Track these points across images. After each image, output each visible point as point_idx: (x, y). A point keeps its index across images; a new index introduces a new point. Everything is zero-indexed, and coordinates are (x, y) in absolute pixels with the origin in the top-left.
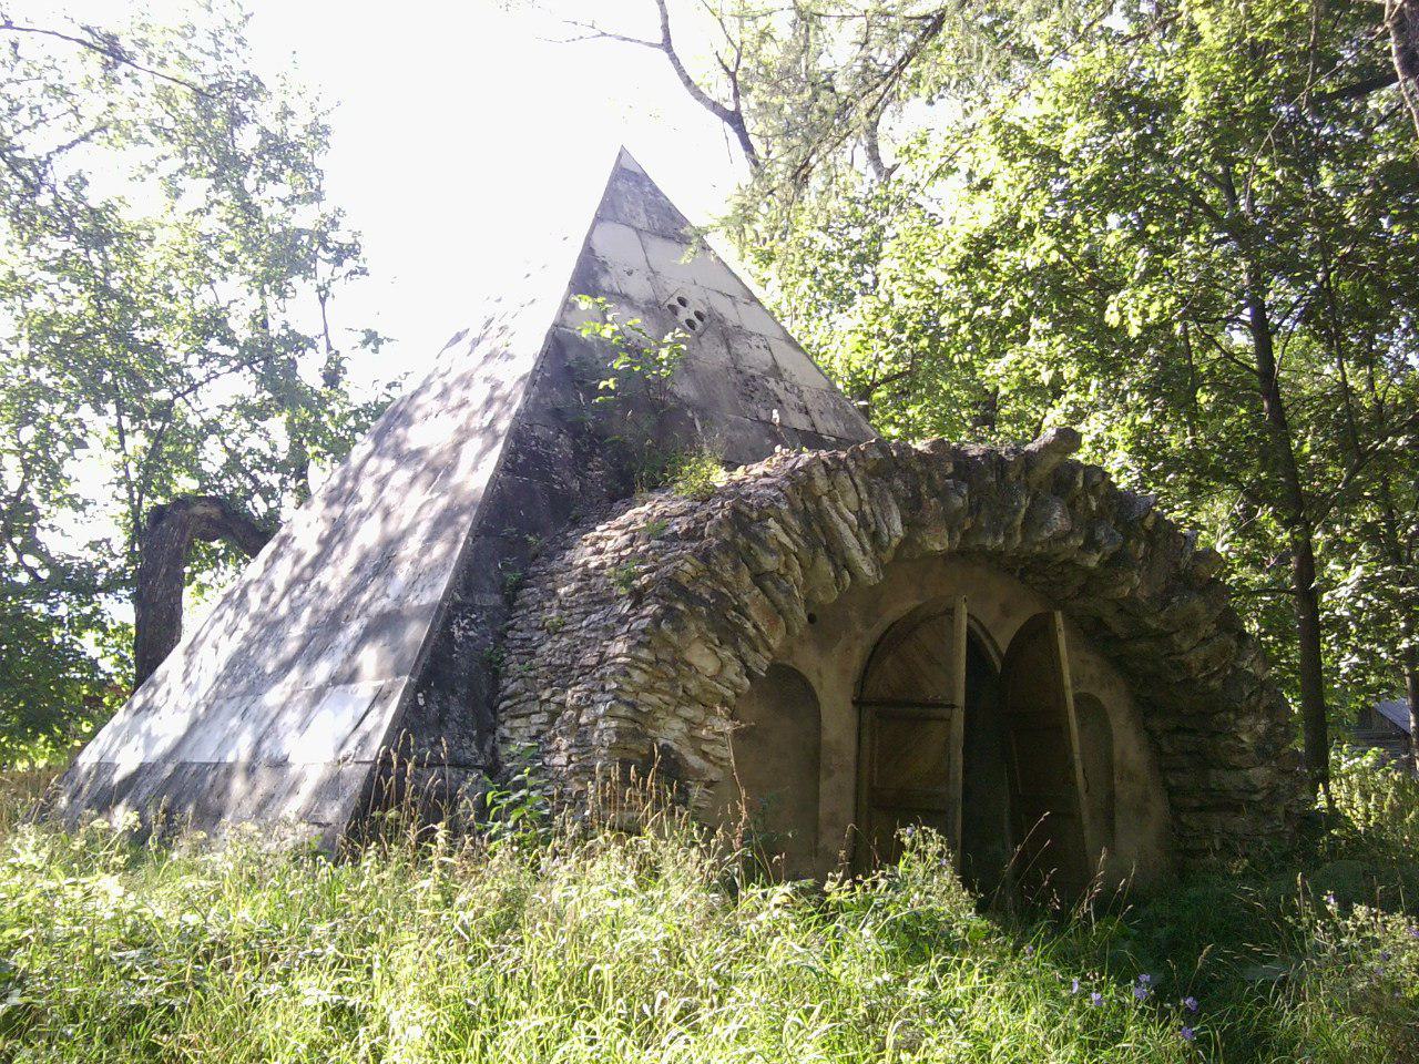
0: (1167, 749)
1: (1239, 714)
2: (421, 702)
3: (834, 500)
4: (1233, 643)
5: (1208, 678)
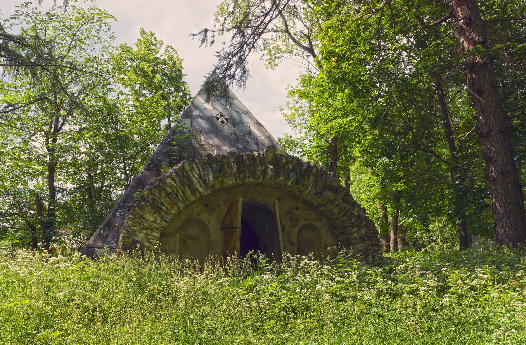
2: (102, 232)
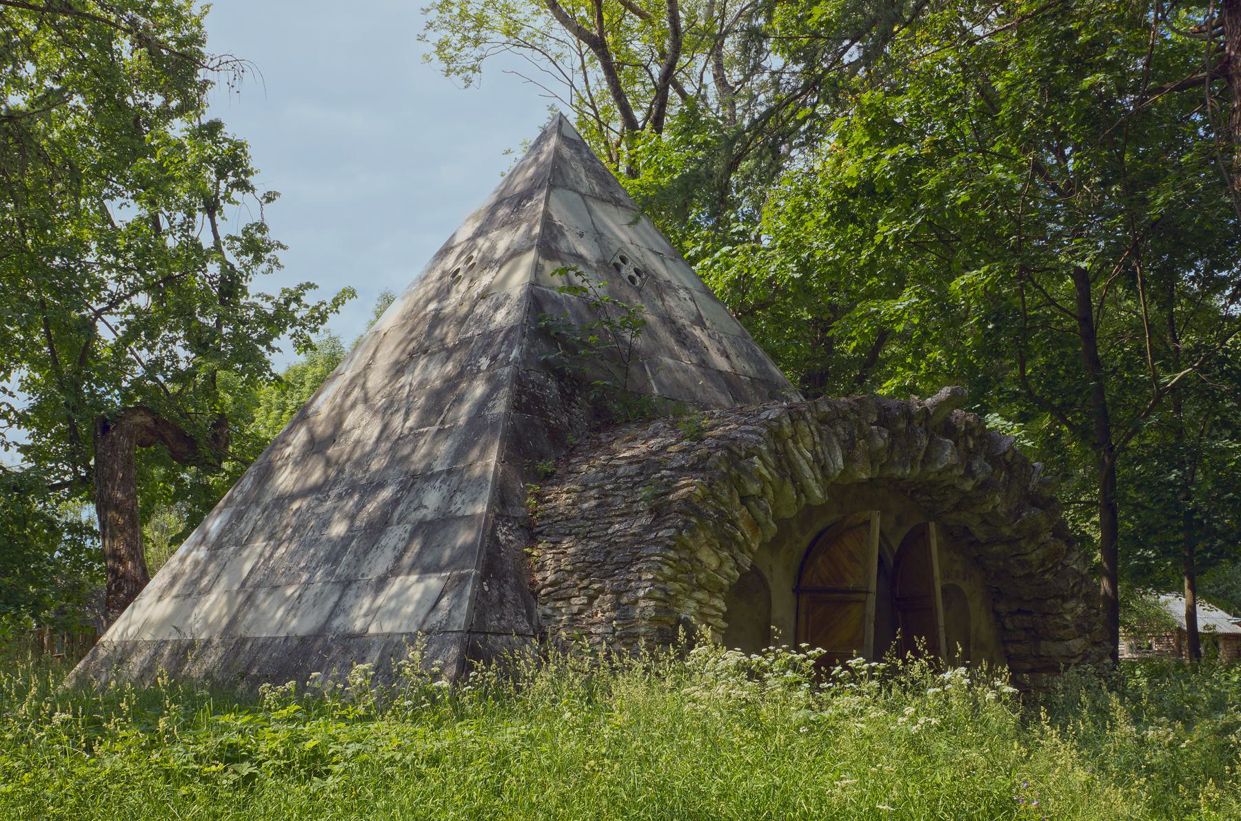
0: (1009, 625)
1: (1065, 599)
2: (486, 589)
3: (796, 443)
4: (1064, 547)
5: (1044, 572)
